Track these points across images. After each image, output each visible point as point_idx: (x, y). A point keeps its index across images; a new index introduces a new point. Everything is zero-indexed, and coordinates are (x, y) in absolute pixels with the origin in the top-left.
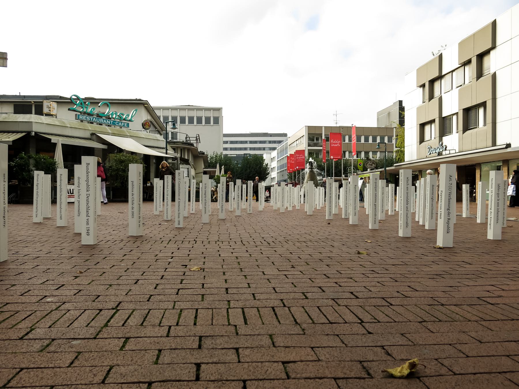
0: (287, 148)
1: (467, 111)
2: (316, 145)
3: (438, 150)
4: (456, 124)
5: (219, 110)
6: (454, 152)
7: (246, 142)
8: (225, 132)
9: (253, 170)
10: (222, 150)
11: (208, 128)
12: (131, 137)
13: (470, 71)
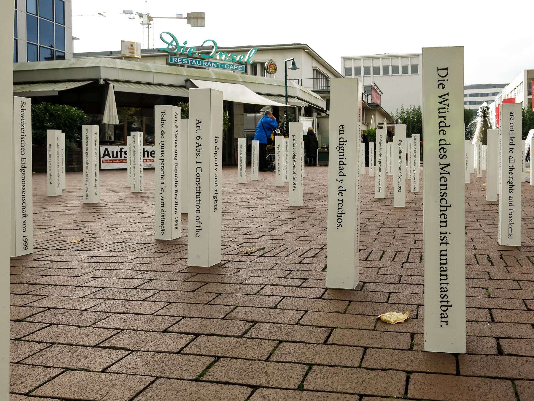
8: (466, 83)
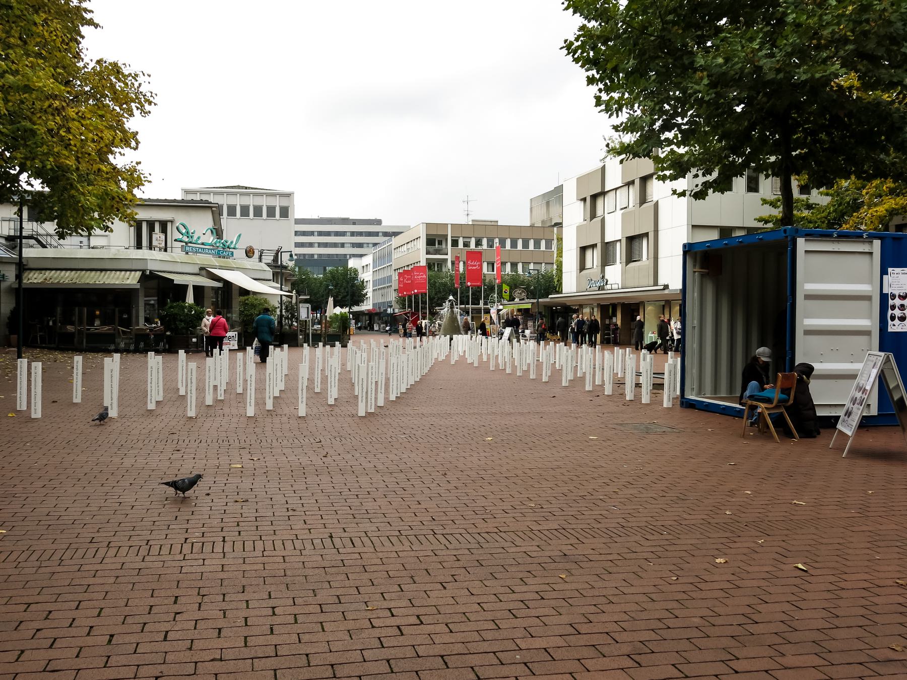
0: (390, 254)
1: (632, 240)
2: (437, 252)
4: (620, 251)
5: (288, 195)
6: (616, 286)
7: (312, 233)
12: (238, 269)
13: (634, 191)
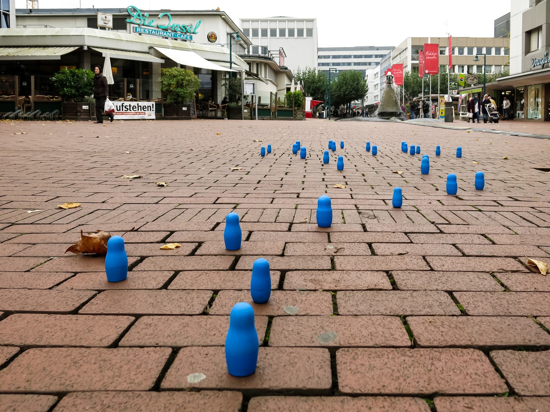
3: (543, 61)
5: (312, 21)
7: (350, 57)
9: (349, 87)
10: (316, 65)
11: (291, 40)
12: (194, 50)
